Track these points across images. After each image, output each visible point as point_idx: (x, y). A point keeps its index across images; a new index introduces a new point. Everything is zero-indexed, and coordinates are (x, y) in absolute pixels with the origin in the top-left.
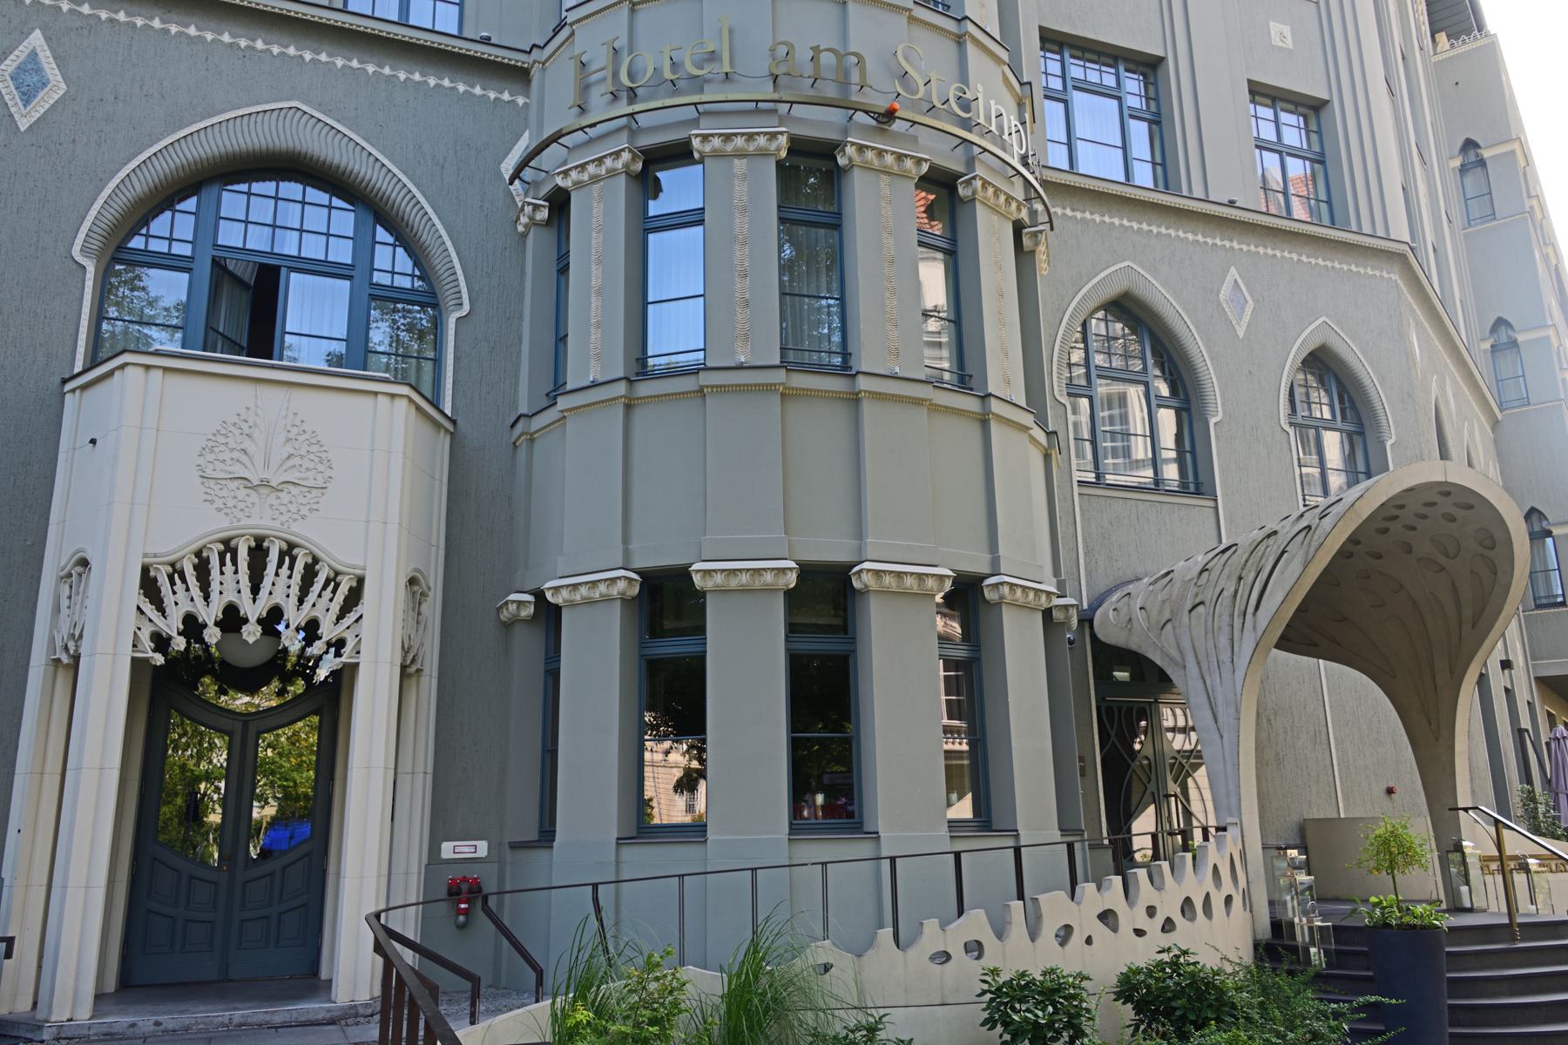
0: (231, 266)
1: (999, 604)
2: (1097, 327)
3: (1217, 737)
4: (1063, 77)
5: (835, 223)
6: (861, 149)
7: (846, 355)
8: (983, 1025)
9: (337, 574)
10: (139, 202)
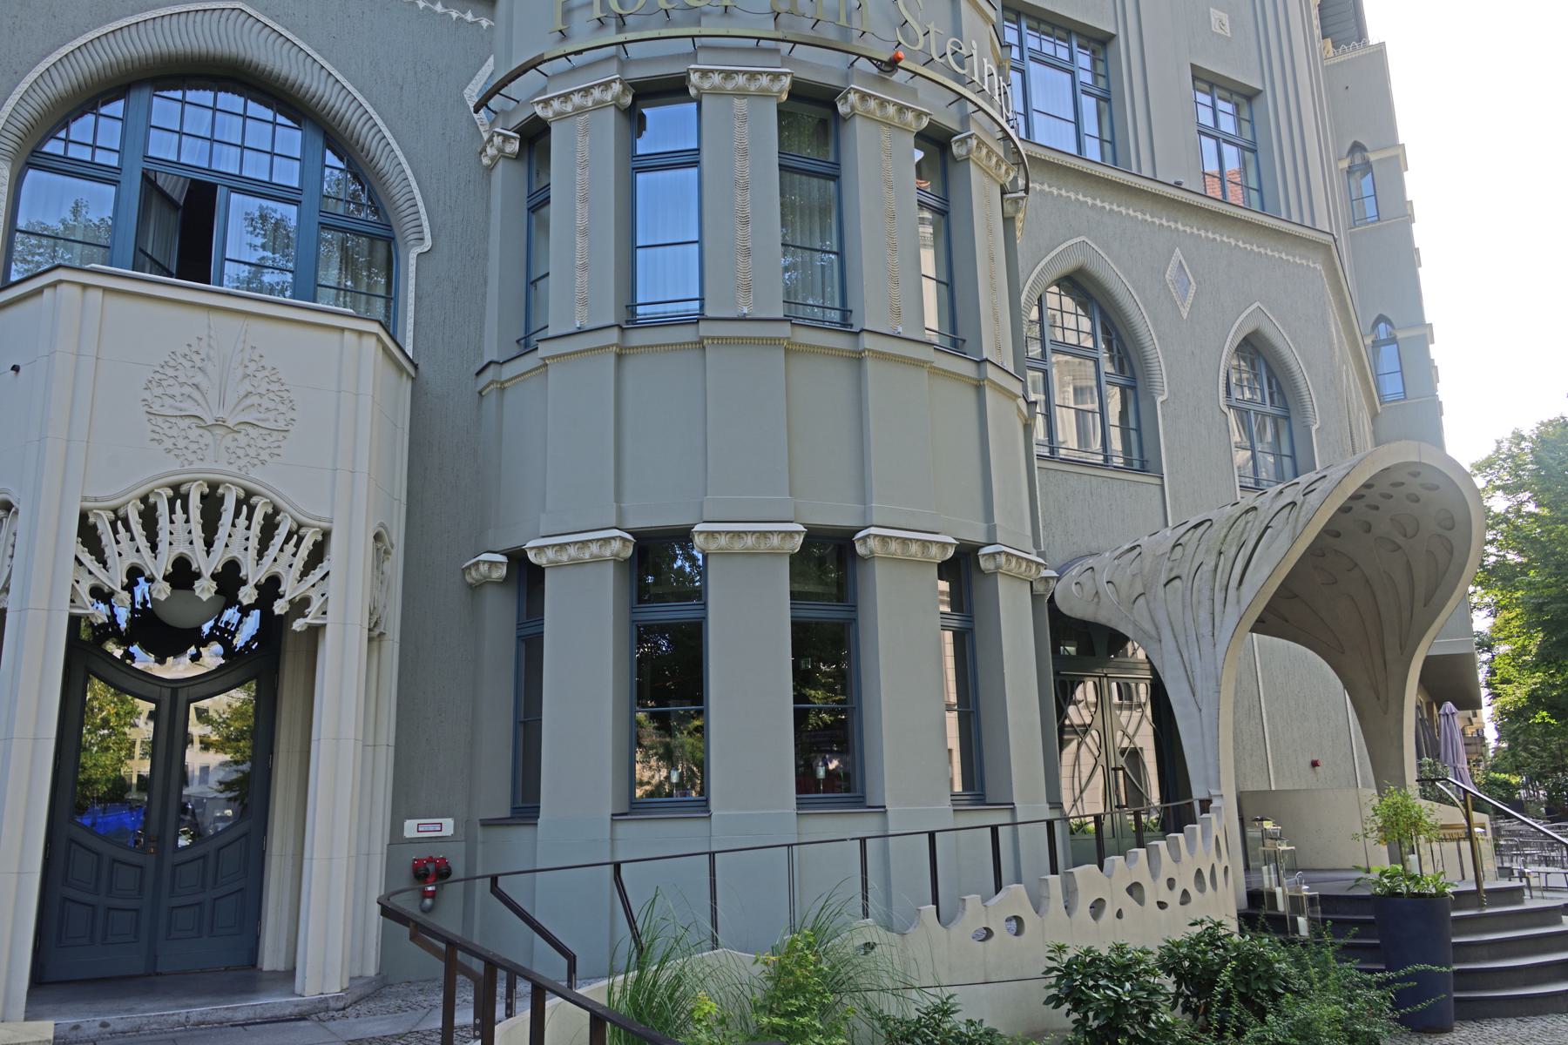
0: (160, 182)
1: (994, 574)
2: (1052, 300)
3: (1195, 710)
4: (1021, 47)
5: (833, 174)
6: (864, 97)
7: (845, 312)
8: (1047, 1003)
9: (300, 526)
10: (60, 102)
